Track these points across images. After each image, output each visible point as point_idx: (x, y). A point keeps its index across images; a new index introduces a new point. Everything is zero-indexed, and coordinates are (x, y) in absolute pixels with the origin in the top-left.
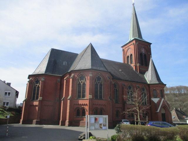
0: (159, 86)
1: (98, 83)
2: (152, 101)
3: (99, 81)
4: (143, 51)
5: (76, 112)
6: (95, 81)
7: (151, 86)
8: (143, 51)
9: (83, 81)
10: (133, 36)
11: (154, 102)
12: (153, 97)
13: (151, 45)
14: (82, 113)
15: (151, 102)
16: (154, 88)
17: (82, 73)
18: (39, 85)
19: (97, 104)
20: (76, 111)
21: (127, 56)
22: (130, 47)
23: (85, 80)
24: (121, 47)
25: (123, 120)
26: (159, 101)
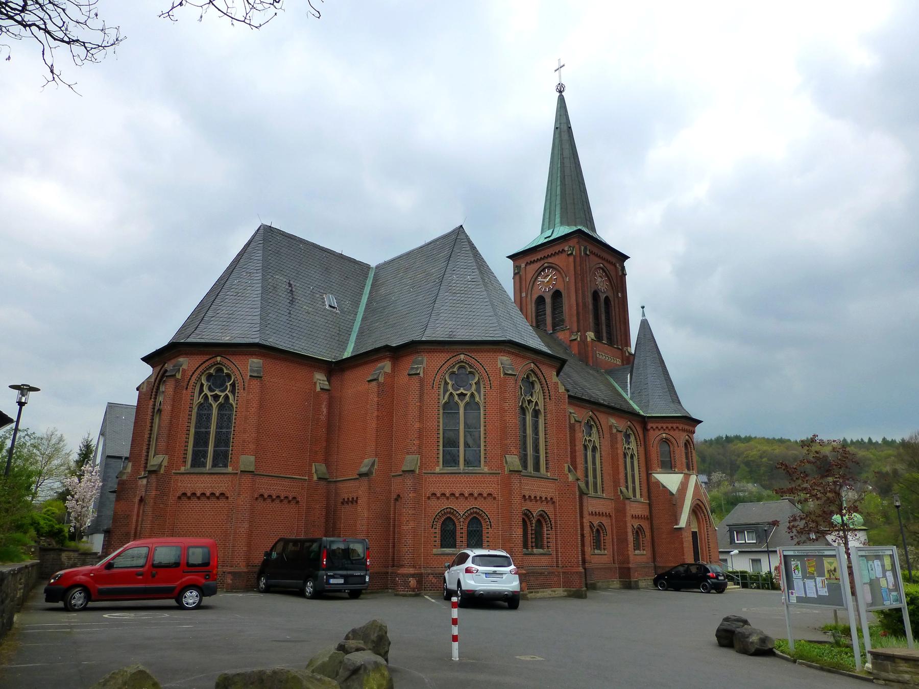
0: (417, 425)
1: (211, 400)
2: (658, 483)
3: (462, 390)
4: (601, 284)
5: (438, 531)
6: (201, 390)
7: (654, 426)
8: (601, 284)
9: (223, 394)
10: (561, 218)
11: (664, 487)
12: (659, 470)
13: (626, 263)
14: (458, 533)
15: (653, 490)
16: (664, 435)
17: (219, 359)
18: (227, 397)
19: (471, 495)
20: (439, 526)
21: (535, 296)
22: (550, 260)
23: (233, 391)
24: (509, 257)
25: (472, 553)
26: (682, 483)
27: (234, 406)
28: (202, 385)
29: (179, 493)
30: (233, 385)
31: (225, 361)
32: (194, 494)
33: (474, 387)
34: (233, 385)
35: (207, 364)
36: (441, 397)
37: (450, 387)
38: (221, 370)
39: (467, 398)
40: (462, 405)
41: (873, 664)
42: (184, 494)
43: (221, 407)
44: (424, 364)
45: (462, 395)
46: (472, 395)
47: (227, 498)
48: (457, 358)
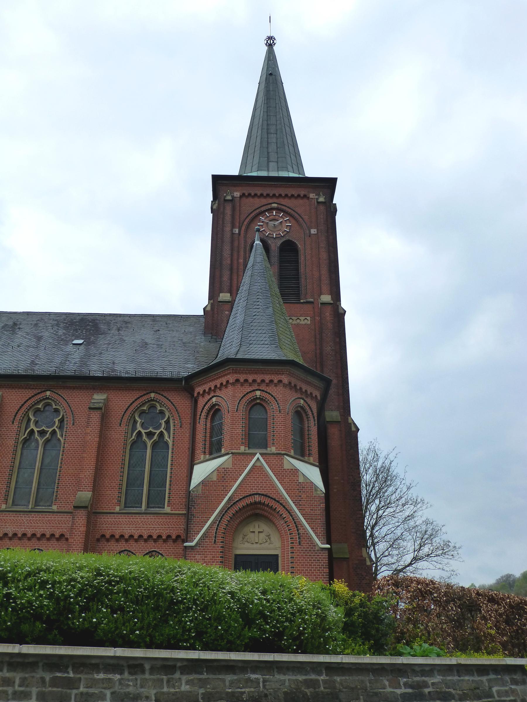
9: (158, 432)
17: (48, 393)
27: (62, 441)
28: (29, 420)
29: (98, 536)
30: (167, 422)
31: (56, 396)
32: (113, 536)
33: (163, 425)
34: (62, 421)
35: (138, 402)
36: (129, 436)
37: (138, 425)
38: (154, 407)
39: (155, 437)
40: (149, 443)
41: (322, 692)
42: (103, 536)
43: (155, 445)
44: (77, 401)
45: (150, 435)
46: (161, 434)
47: (67, 539)
48: (42, 395)
